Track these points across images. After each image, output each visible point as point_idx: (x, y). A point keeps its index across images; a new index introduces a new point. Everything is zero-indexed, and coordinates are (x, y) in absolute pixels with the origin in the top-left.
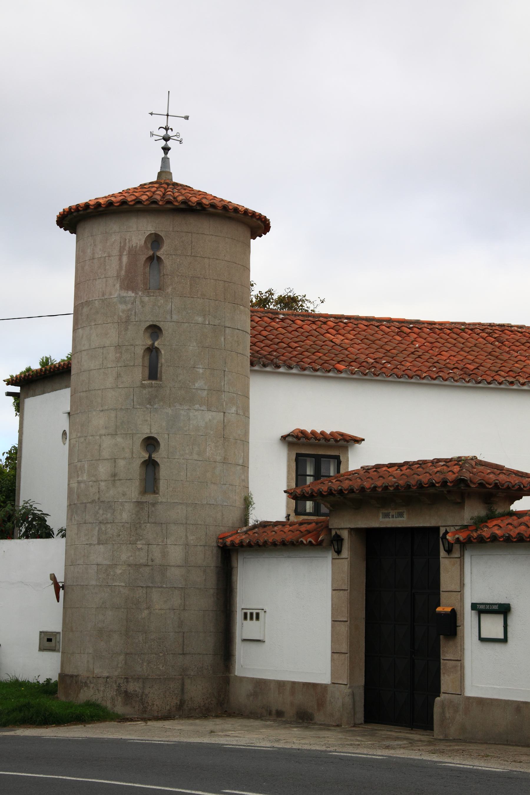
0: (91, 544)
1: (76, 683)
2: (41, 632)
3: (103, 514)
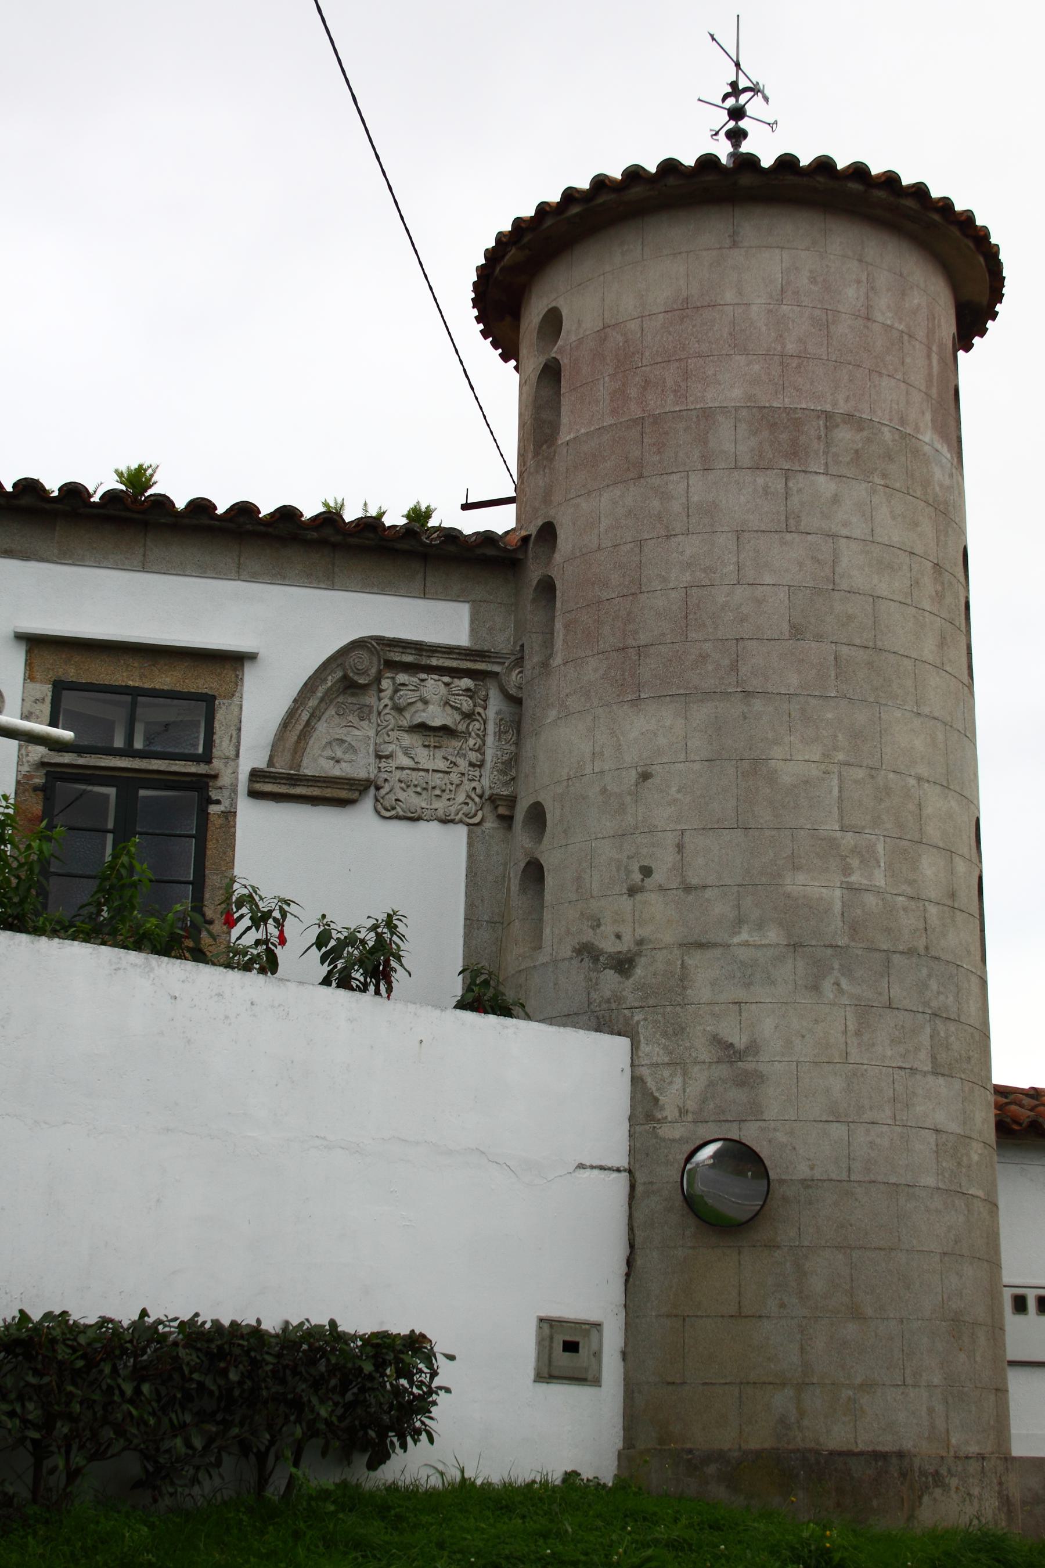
0: (913, 1070)
1: (903, 1475)
2: (541, 1320)
3: (939, 993)
